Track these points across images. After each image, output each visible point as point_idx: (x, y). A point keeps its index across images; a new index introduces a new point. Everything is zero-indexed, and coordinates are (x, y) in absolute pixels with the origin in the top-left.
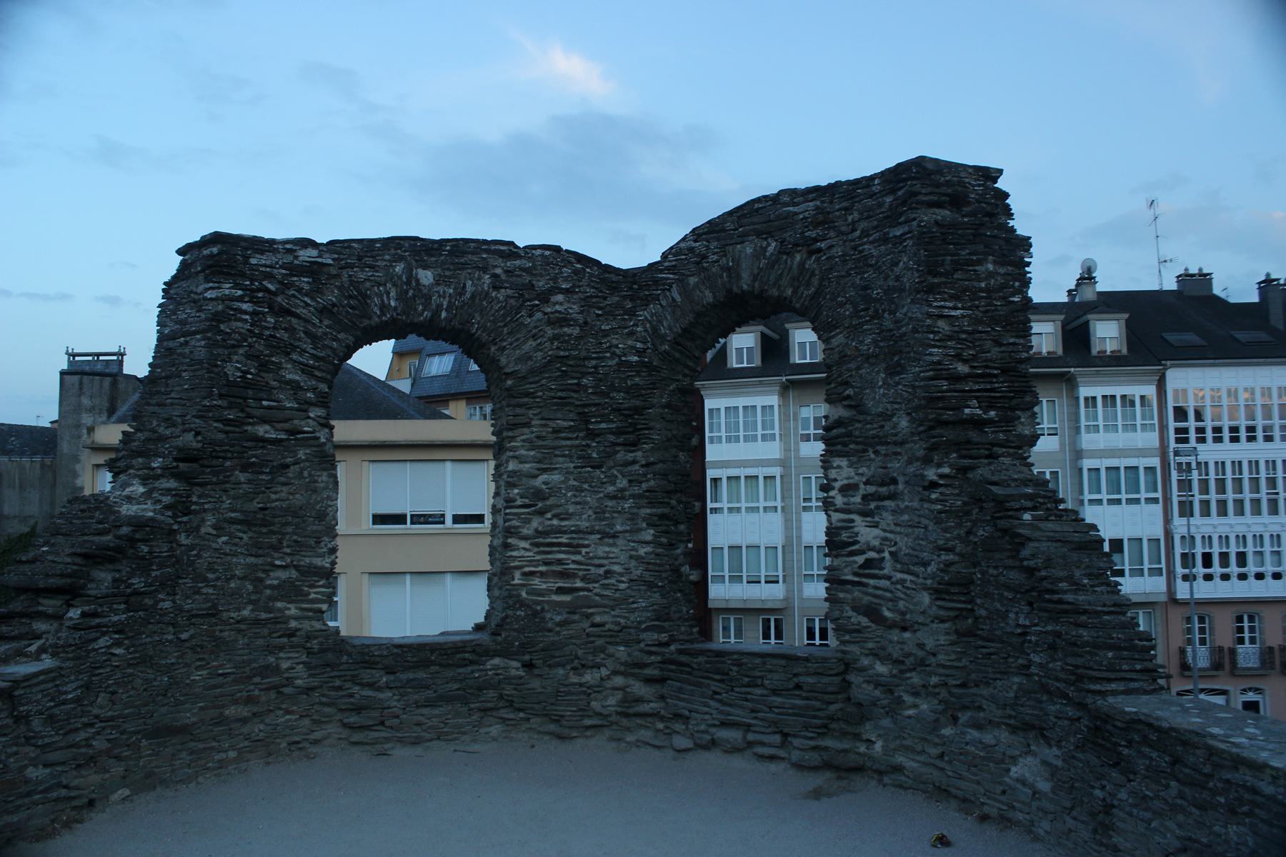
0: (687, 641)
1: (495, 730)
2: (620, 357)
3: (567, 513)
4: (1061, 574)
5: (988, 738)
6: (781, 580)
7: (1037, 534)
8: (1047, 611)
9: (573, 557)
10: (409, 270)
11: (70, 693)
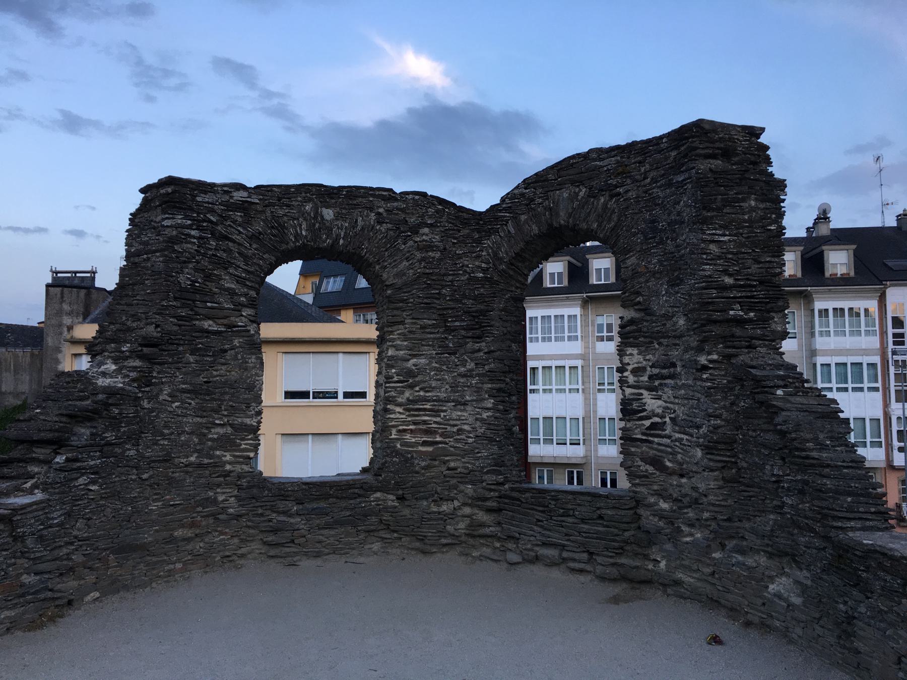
0: (517, 482)
1: (376, 546)
2: (469, 274)
3: (430, 387)
4: (809, 436)
5: (750, 562)
6: (581, 442)
7: (789, 405)
8: (797, 465)
9: (435, 419)
10: (316, 209)
11: (56, 519)
